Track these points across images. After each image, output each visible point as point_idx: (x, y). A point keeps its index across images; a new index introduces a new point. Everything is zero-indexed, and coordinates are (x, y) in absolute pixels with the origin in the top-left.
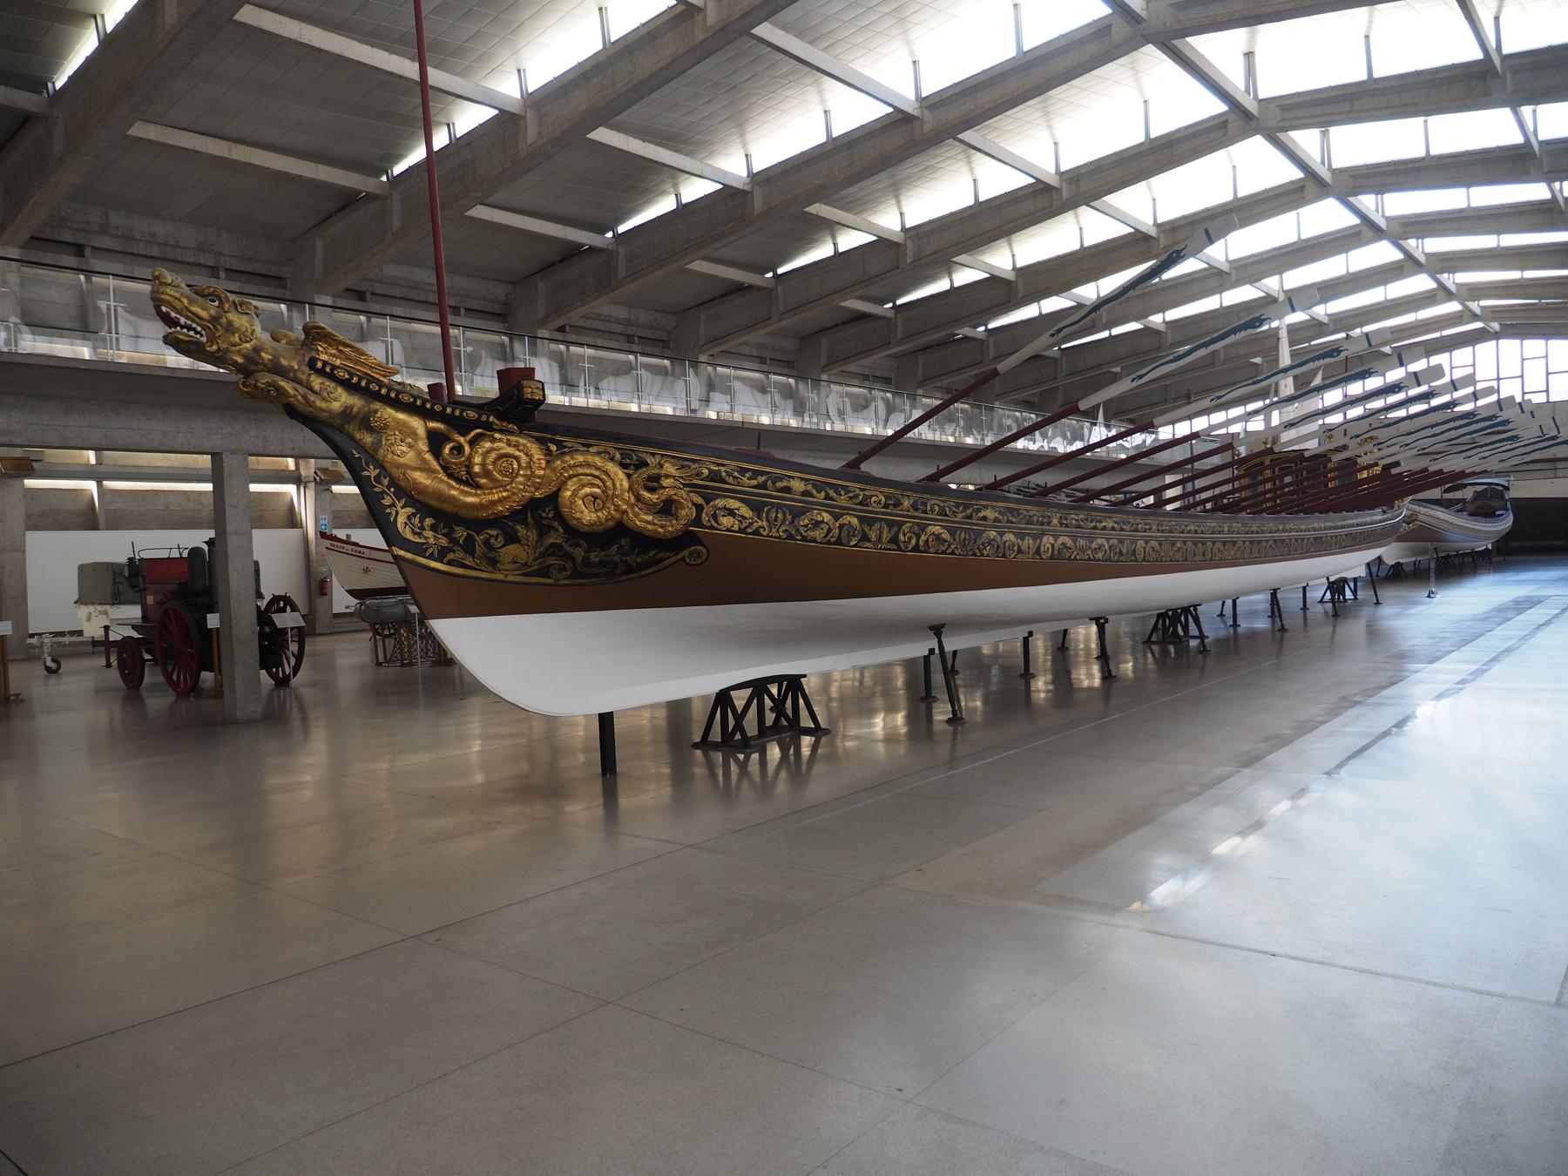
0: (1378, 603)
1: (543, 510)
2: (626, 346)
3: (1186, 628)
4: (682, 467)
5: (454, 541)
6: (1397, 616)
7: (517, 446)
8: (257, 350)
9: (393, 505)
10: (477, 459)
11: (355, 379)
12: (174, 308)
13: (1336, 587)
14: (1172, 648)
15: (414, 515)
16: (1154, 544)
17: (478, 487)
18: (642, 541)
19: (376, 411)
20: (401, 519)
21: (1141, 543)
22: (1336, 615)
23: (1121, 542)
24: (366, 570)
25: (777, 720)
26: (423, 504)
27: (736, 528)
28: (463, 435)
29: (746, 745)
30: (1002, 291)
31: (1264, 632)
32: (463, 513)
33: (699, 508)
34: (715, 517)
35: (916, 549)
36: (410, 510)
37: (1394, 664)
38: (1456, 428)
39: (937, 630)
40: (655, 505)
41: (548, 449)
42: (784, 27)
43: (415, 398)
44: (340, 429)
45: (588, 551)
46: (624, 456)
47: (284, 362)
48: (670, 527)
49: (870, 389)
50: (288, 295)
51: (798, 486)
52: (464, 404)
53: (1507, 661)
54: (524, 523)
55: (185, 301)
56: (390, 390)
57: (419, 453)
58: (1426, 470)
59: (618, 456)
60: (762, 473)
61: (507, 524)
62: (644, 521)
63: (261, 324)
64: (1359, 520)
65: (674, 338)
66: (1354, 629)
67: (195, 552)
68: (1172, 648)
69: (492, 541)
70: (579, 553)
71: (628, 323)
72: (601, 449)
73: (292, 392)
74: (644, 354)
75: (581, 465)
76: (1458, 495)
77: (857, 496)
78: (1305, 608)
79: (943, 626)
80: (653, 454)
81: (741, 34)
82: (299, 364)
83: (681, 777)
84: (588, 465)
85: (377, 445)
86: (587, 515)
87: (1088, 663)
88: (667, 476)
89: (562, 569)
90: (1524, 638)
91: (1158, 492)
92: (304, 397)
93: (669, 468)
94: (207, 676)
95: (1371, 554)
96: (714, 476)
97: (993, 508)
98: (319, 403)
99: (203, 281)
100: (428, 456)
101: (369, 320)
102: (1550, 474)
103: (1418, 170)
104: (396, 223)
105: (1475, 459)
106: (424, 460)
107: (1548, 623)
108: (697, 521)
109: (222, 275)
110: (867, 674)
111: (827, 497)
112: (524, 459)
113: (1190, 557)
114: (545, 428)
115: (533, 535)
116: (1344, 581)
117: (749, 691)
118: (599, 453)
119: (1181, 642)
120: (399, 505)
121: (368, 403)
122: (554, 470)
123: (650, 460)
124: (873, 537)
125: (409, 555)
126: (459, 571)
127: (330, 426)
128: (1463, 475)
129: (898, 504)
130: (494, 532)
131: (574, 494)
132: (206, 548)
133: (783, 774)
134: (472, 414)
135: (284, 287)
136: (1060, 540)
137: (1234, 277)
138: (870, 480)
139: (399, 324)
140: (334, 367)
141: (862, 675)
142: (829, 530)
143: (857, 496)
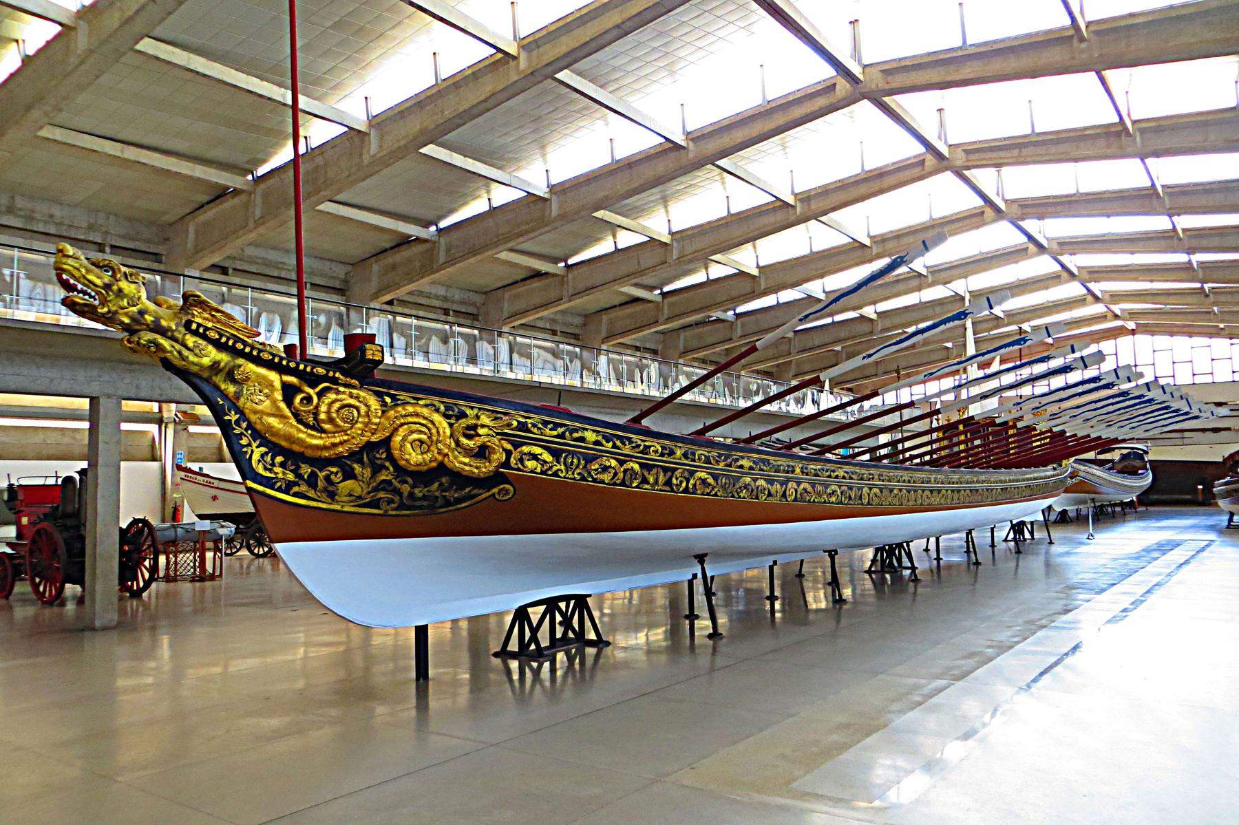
0: (1051, 543)
1: (377, 452)
2: (443, 318)
3: (899, 560)
4: (496, 419)
6: (1068, 553)
7: (357, 398)
8: (142, 313)
9: (249, 445)
10: (323, 408)
11: (224, 340)
12: (73, 276)
13: (1018, 528)
14: (888, 576)
15: (266, 453)
16: (876, 490)
17: (323, 431)
18: (459, 479)
19: (240, 366)
20: (256, 457)
21: (866, 490)
22: (1018, 552)
23: (850, 488)
24: (215, 498)
25: (565, 634)
26: (275, 444)
27: (539, 470)
28: (313, 388)
29: (540, 654)
30: (748, 284)
31: (958, 565)
32: (309, 453)
33: (509, 453)
34: (521, 460)
35: (686, 490)
36: (263, 449)
37: (1067, 597)
38: (1113, 404)
39: (701, 558)
40: (471, 449)
41: (384, 401)
42: (580, 74)
43: (274, 355)
44: (208, 380)
45: (413, 487)
46: (447, 409)
47: (164, 323)
49: (641, 358)
50: (162, 268)
51: (591, 436)
52: (316, 362)
53: (1158, 593)
54: (361, 462)
55: (83, 271)
56: (253, 348)
58: (1089, 436)
59: (442, 408)
60: (561, 425)
61: (345, 464)
62: (461, 462)
63: (136, 292)
64: (1036, 475)
65: (479, 313)
66: (1034, 564)
67: (68, 480)
68: (888, 576)
69: (333, 477)
70: (406, 489)
71: (445, 299)
72: (428, 402)
73: (168, 348)
74: (460, 325)
75: (411, 415)
76: (1108, 456)
77: (639, 446)
78: (993, 546)
79: (706, 555)
80: (472, 408)
81: (547, 77)
82: (177, 325)
83: (478, 683)
84: (417, 415)
85: (238, 395)
86: (414, 457)
87: (816, 590)
88: (483, 426)
89: (390, 502)
90: (1170, 575)
91: (872, 450)
92: (180, 353)
93: (485, 419)
94: (71, 589)
95: (1045, 503)
96: (522, 427)
97: (749, 458)
98: (192, 358)
99: (97, 256)
100: (283, 405)
101: (229, 290)
102: (1179, 442)
103: (1070, 203)
104: (258, 213)
105: (1126, 429)
106: (278, 408)
107: (1186, 562)
108: (506, 464)
109: (108, 249)
110: (635, 596)
111: (614, 446)
112: (363, 410)
113: (904, 502)
114: (382, 383)
115: (368, 472)
116: (1023, 523)
117: (543, 607)
118: (426, 406)
119: (896, 571)
120: (254, 445)
121: (234, 359)
122: (388, 418)
123: (468, 412)
124: (651, 480)
125: (260, 488)
126: (303, 502)
127: (200, 377)
128: (1116, 441)
129: (672, 453)
130: (334, 470)
131: (404, 439)
132: (77, 477)
133: (570, 680)
134: (321, 371)
135: (160, 262)
136: (802, 486)
137: (930, 279)
138: (648, 433)
139: (257, 295)
140: (207, 329)
141: (631, 595)
142: (616, 474)
143: (639, 446)
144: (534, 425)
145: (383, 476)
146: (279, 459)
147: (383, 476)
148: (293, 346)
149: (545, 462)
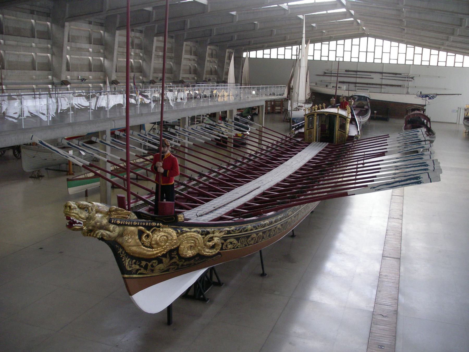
5: (141, 266)
34: (227, 246)
36: (129, 259)
38: (414, 171)
41: (178, 231)
48: (214, 252)
57: (136, 240)
62: (207, 252)
69: (154, 264)
88: (216, 236)
100: (138, 241)
144: (232, 230)
145: (173, 261)
146: (134, 261)
147: (173, 261)
148: (123, 198)
149: (234, 244)
